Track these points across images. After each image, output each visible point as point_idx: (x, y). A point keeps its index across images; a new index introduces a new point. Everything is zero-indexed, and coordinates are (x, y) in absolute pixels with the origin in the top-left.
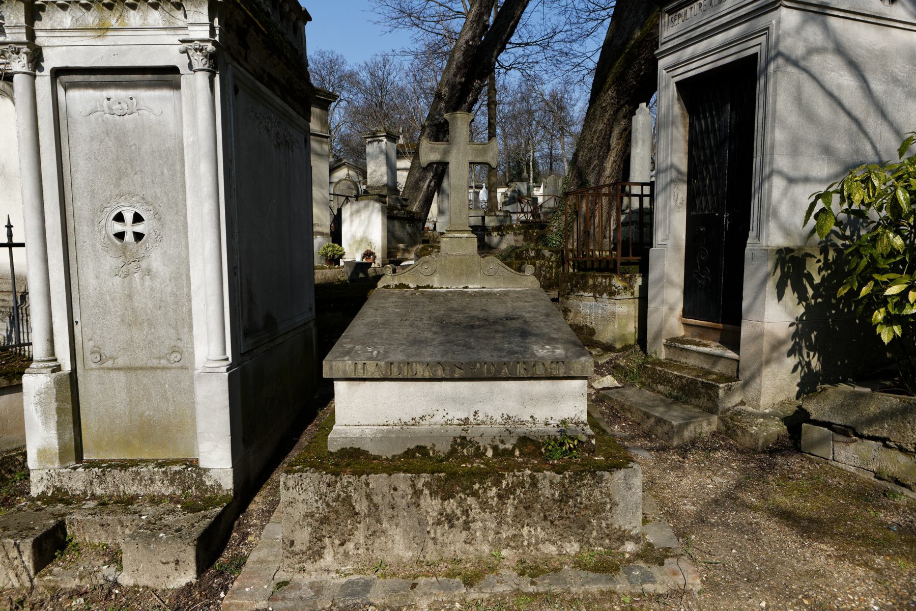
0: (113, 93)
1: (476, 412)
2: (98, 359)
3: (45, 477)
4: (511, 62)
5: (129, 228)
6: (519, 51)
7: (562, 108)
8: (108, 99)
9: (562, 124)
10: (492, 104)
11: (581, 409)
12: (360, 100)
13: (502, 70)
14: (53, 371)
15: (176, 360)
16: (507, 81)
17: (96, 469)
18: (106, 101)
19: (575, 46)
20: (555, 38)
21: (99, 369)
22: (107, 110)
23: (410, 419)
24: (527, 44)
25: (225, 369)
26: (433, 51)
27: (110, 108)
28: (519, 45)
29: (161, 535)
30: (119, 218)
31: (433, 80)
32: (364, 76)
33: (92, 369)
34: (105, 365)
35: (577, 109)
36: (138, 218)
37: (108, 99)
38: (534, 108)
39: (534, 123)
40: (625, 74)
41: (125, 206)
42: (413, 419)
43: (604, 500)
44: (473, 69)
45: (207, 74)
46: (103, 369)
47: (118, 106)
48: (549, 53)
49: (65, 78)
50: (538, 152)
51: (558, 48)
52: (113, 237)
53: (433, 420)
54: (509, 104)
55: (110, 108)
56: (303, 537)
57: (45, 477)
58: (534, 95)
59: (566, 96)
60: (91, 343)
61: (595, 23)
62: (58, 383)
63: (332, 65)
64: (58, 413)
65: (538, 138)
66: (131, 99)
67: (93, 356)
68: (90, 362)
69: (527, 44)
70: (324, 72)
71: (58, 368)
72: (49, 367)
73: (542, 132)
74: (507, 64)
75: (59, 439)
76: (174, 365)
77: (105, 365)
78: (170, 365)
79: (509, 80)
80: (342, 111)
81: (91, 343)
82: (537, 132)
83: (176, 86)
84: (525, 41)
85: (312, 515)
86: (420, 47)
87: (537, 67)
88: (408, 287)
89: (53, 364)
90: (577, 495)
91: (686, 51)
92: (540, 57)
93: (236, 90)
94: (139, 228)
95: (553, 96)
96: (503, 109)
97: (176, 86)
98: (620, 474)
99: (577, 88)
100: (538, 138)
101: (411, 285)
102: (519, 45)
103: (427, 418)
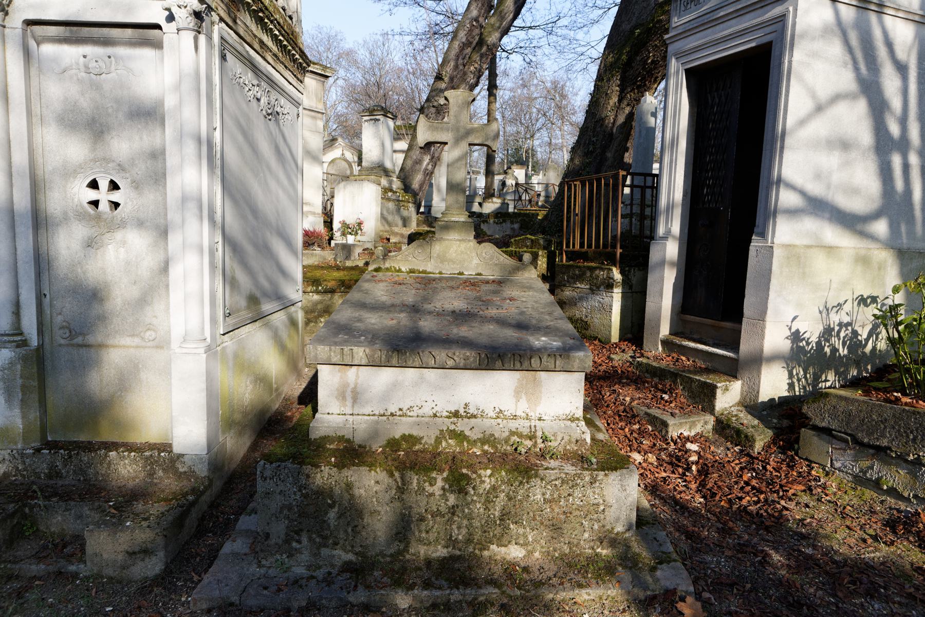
0: (89, 49)
1: (466, 405)
2: (67, 335)
3: (7, 457)
4: (513, 46)
5: (103, 195)
6: (522, 34)
7: (563, 96)
8: (85, 57)
9: (562, 111)
10: (492, 87)
11: (577, 405)
12: (358, 78)
13: (504, 54)
14: (18, 346)
15: (151, 338)
16: (508, 66)
17: (62, 451)
18: (82, 59)
19: (580, 35)
20: (559, 23)
21: (68, 345)
22: (82, 69)
23: (397, 410)
24: (530, 28)
25: (202, 351)
26: (434, 32)
27: (86, 67)
28: (522, 28)
29: (128, 524)
30: (94, 185)
31: (432, 60)
32: (363, 55)
33: (60, 345)
34: (75, 341)
35: (579, 98)
36: (114, 186)
37: (85, 57)
38: (535, 95)
39: (534, 110)
40: (632, 57)
41: (100, 172)
42: (400, 410)
43: (596, 501)
44: (474, 53)
45: (191, 34)
46: (73, 345)
47: (95, 64)
48: (553, 38)
49: (38, 29)
50: (538, 144)
51: (564, 34)
52: (87, 206)
53: (421, 412)
54: (511, 90)
55: (86, 67)
56: (279, 529)
57: (7, 457)
58: (535, 82)
59: (568, 84)
60: (60, 318)
61: (601, 12)
62: (25, 359)
63: (331, 41)
64: (22, 391)
65: (539, 125)
66: (109, 57)
67: (61, 331)
68: (59, 338)
69: (530, 28)
70: (321, 49)
71: (24, 343)
72: (14, 341)
73: (542, 120)
74: (508, 48)
75: (23, 418)
76: (149, 344)
77: (75, 341)
78: (144, 344)
79: (510, 66)
80: (339, 90)
81: (60, 318)
82: (537, 120)
83: (158, 45)
84: (528, 25)
85: (290, 508)
86: (422, 27)
87: (539, 52)
88: (399, 271)
89: (19, 338)
90: (569, 495)
91: (702, 37)
92: (543, 42)
93: (223, 57)
94: (115, 196)
95: (555, 83)
96: (503, 94)
97: (158, 45)
98: (614, 477)
99: (580, 77)
100: (539, 125)
101: (403, 269)
102: (522, 28)
103: (415, 408)
